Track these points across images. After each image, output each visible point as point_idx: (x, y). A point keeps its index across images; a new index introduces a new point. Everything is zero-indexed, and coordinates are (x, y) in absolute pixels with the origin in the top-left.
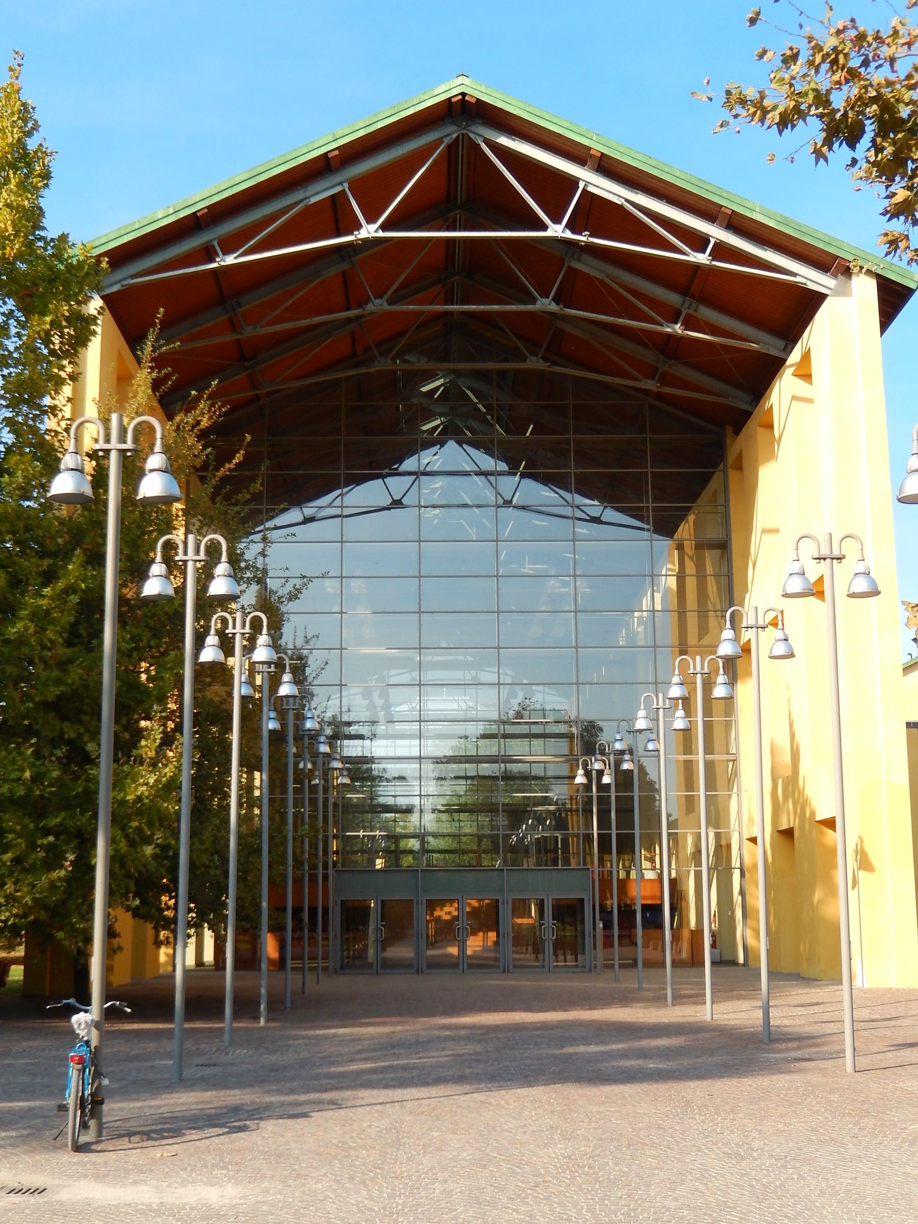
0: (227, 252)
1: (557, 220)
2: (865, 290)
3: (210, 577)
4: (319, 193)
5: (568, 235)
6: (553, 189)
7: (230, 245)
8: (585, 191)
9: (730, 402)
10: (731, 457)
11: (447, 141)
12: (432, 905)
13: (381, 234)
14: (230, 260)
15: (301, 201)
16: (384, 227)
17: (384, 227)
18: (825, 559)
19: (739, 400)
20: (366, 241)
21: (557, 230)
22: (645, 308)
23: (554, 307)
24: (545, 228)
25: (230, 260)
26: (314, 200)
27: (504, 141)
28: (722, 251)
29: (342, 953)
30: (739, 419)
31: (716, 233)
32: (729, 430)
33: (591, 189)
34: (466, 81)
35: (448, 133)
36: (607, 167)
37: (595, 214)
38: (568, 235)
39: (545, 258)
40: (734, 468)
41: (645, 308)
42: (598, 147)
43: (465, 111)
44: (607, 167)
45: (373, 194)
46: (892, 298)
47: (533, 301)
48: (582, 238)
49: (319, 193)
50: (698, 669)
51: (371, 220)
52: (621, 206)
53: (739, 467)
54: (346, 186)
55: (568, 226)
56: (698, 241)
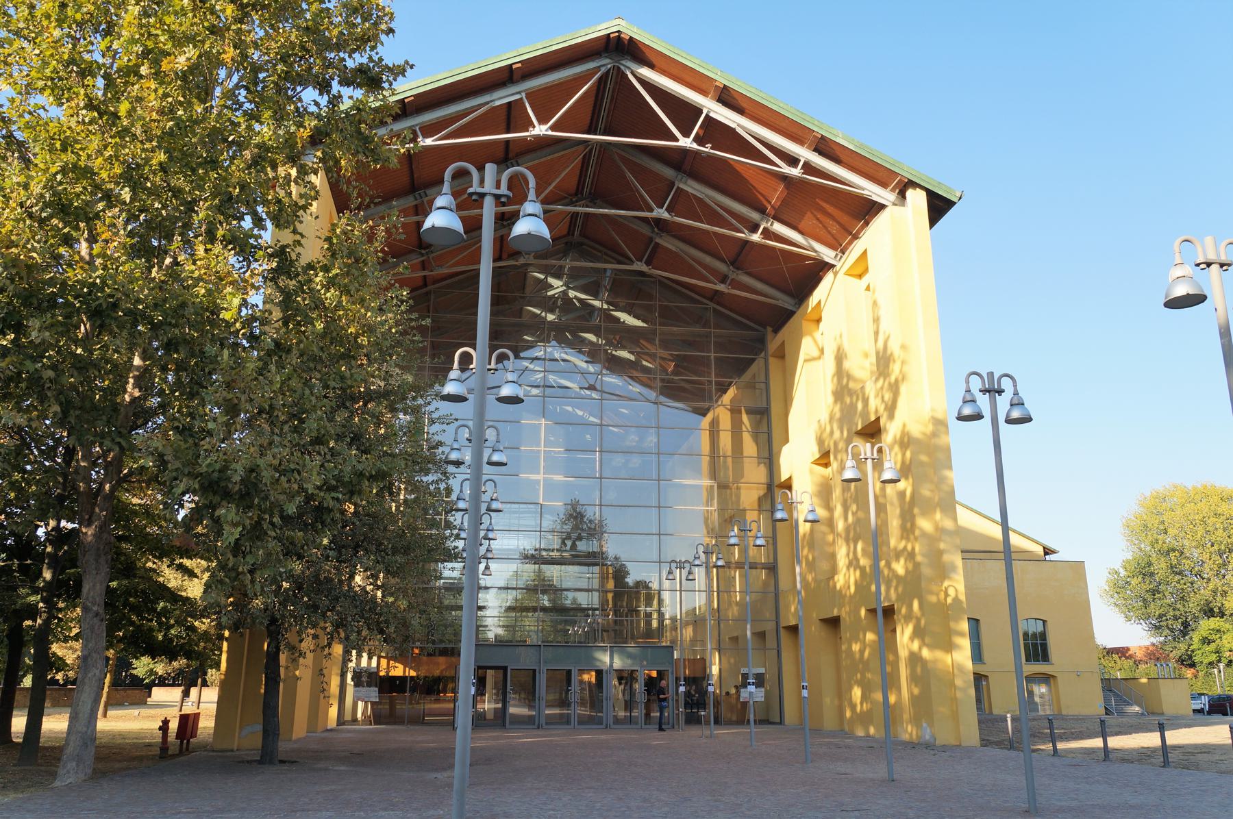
0: (425, 136)
1: (686, 134)
2: (917, 199)
3: (513, 217)
4: (501, 98)
5: (695, 146)
6: (685, 114)
7: (428, 131)
8: (707, 116)
9: (780, 303)
10: (773, 345)
11: (603, 70)
12: (582, 671)
13: (550, 133)
14: (429, 142)
15: (488, 103)
16: (553, 128)
17: (553, 128)
18: (1209, 265)
19: (784, 301)
20: (537, 137)
21: (686, 142)
22: (734, 221)
23: (666, 215)
24: (677, 140)
25: (429, 142)
26: (498, 103)
27: (645, 72)
28: (809, 168)
29: (552, 721)
30: (781, 318)
31: (805, 154)
32: (769, 329)
33: (712, 115)
34: (623, 23)
35: (605, 63)
36: (726, 97)
37: (715, 132)
38: (695, 146)
39: (680, 160)
40: (774, 356)
41: (734, 221)
42: (722, 79)
43: (621, 47)
44: (726, 97)
45: (545, 104)
46: (938, 206)
47: (651, 210)
48: (707, 149)
49: (501, 98)
50: (869, 454)
51: (542, 121)
52: (734, 130)
53: (781, 355)
54: (524, 95)
55: (695, 140)
56: (792, 161)
